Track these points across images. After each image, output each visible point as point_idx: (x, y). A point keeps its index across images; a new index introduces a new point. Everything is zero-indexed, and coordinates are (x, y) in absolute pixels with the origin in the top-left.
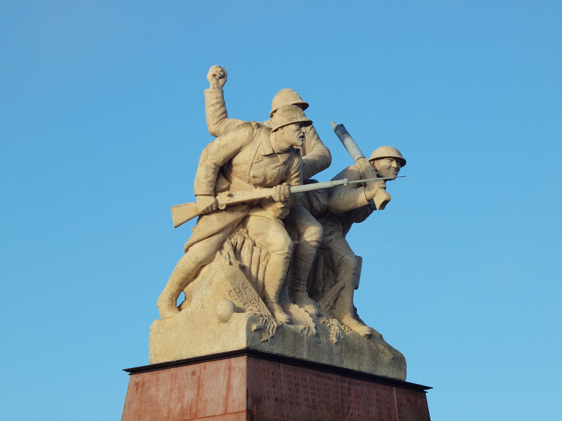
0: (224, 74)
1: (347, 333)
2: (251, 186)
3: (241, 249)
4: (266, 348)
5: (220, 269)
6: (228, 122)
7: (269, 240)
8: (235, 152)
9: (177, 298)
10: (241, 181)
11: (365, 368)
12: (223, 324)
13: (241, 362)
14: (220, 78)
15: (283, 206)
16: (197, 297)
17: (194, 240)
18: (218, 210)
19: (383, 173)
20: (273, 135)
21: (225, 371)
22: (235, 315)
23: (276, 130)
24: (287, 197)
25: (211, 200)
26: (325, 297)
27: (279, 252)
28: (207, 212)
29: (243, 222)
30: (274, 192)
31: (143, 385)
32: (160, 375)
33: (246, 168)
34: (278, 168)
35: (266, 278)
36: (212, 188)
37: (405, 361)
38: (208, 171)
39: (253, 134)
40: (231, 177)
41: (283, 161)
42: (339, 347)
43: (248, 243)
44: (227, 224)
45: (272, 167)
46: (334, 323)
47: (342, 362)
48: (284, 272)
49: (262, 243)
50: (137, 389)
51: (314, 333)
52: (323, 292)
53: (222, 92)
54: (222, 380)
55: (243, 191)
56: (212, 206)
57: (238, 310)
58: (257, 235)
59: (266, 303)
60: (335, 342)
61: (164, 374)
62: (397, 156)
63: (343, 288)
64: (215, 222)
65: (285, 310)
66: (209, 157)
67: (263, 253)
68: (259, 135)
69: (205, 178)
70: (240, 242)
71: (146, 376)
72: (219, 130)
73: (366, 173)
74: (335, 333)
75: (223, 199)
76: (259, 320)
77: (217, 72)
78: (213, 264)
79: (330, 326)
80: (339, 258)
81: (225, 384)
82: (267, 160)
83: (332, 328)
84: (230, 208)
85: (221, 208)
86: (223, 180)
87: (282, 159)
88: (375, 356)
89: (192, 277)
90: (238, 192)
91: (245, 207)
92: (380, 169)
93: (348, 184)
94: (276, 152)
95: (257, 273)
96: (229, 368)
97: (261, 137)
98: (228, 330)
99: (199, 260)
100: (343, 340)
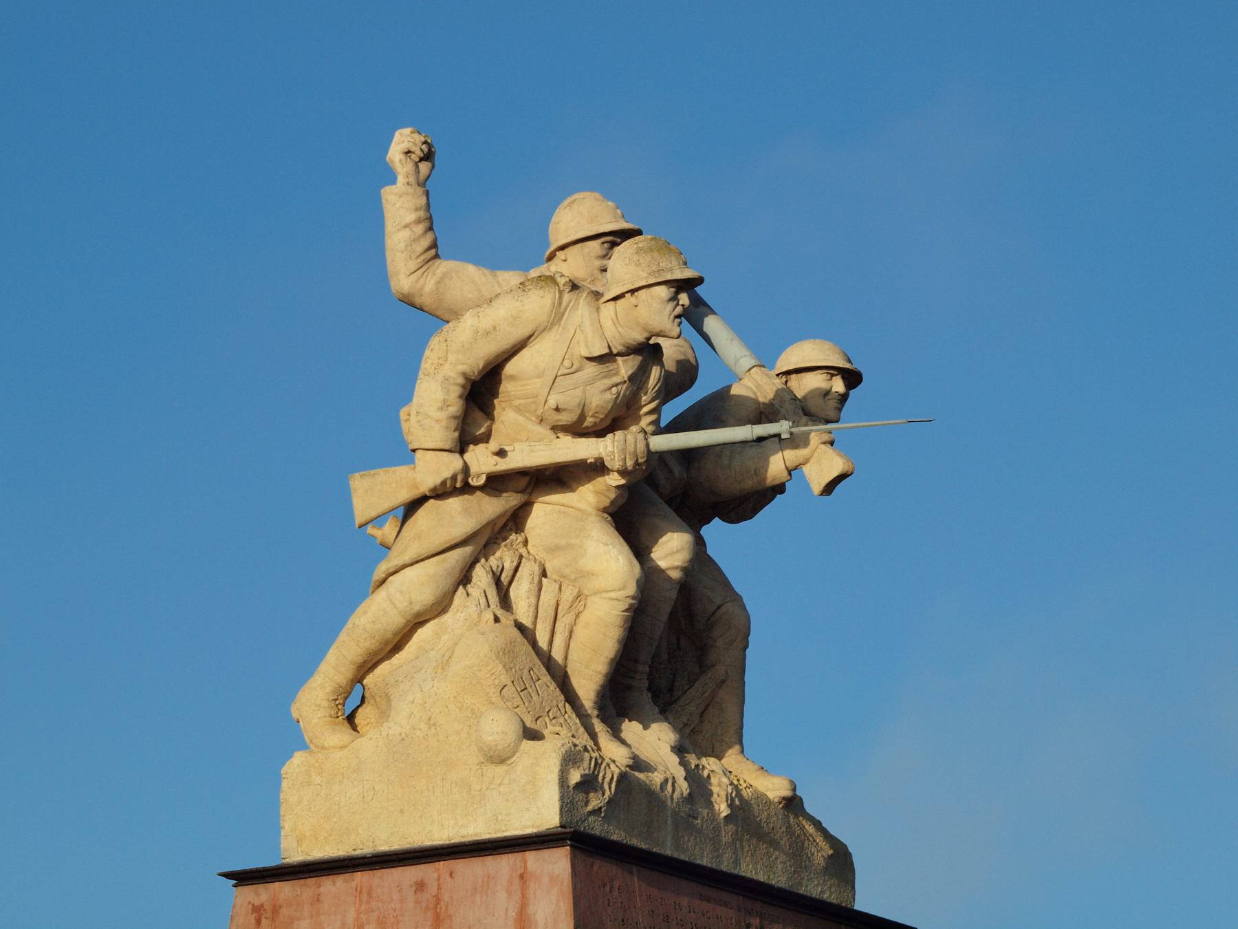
0: (430, 150)
1: (744, 793)
2: (544, 431)
3: (510, 583)
4: (596, 827)
5: (467, 636)
6: (439, 272)
7: (587, 563)
8: (514, 346)
9: (346, 698)
10: (521, 419)
11: (779, 878)
12: (493, 766)
13: (558, 862)
14: (421, 160)
15: (623, 482)
16: (410, 698)
17: (407, 558)
18: (467, 489)
19: (813, 405)
20: (608, 310)
21: (510, 883)
22: (527, 745)
23: (615, 299)
24: (641, 461)
25: (453, 463)
26: (681, 702)
27: (613, 595)
28: (441, 492)
29: (515, 520)
30: (610, 448)
31: (276, 910)
32: (322, 889)
33: (538, 386)
34: (614, 390)
35: (573, 655)
36: (457, 434)
37: (852, 864)
38: (448, 392)
39: (560, 304)
40: (493, 407)
41: (630, 372)
42: (731, 827)
43: (528, 571)
44: (484, 522)
45: (602, 387)
46: (714, 768)
47: (737, 862)
48: (619, 641)
49: (567, 571)
50: (259, 922)
51: (686, 793)
52: (671, 690)
53: (427, 194)
54: (503, 904)
55: (523, 441)
56: (454, 478)
57: (532, 735)
58: (554, 549)
59: (579, 716)
60: (724, 814)
61: (333, 886)
62: (847, 366)
63: (723, 682)
64: (458, 517)
65: (616, 734)
66: (451, 358)
67: (568, 594)
68: (575, 308)
69: (441, 409)
70: (509, 565)
71: (283, 890)
72: (422, 289)
73: (776, 403)
74: (723, 794)
75: (481, 461)
76: (582, 760)
77: (415, 144)
78: (447, 618)
79: (709, 776)
80: (712, 608)
81: (513, 914)
82: (592, 369)
83: (714, 780)
84: (496, 483)
85: (474, 482)
86: (478, 415)
87: (625, 367)
88: (798, 852)
89: (388, 648)
90: (517, 445)
91: (524, 482)
92: (805, 398)
93: (791, 434)
94: (615, 351)
95: (551, 642)
96: (522, 877)
97: (580, 311)
98: (506, 781)
99: (417, 608)
100: (744, 810)
